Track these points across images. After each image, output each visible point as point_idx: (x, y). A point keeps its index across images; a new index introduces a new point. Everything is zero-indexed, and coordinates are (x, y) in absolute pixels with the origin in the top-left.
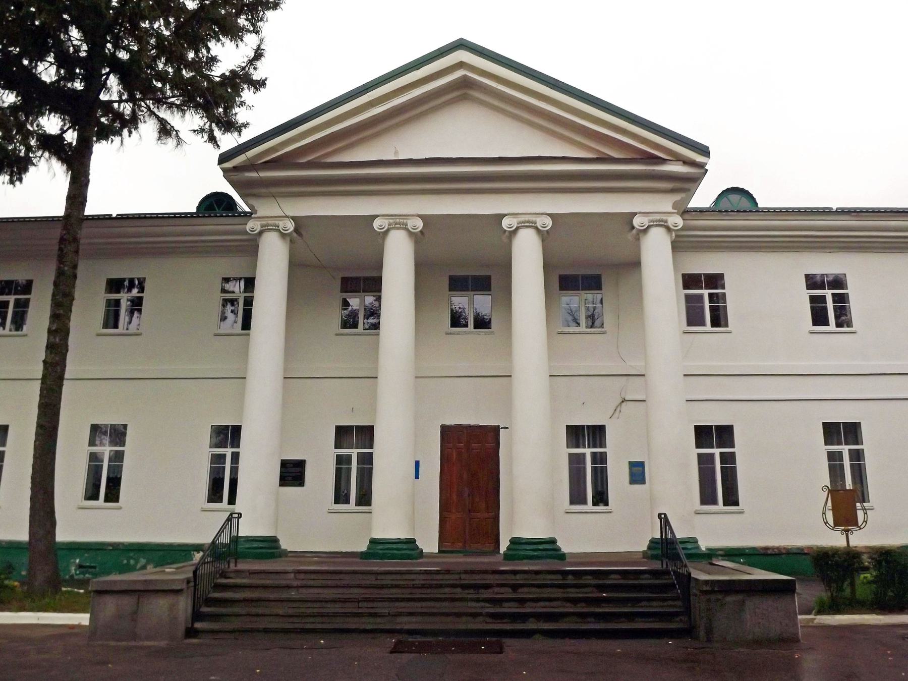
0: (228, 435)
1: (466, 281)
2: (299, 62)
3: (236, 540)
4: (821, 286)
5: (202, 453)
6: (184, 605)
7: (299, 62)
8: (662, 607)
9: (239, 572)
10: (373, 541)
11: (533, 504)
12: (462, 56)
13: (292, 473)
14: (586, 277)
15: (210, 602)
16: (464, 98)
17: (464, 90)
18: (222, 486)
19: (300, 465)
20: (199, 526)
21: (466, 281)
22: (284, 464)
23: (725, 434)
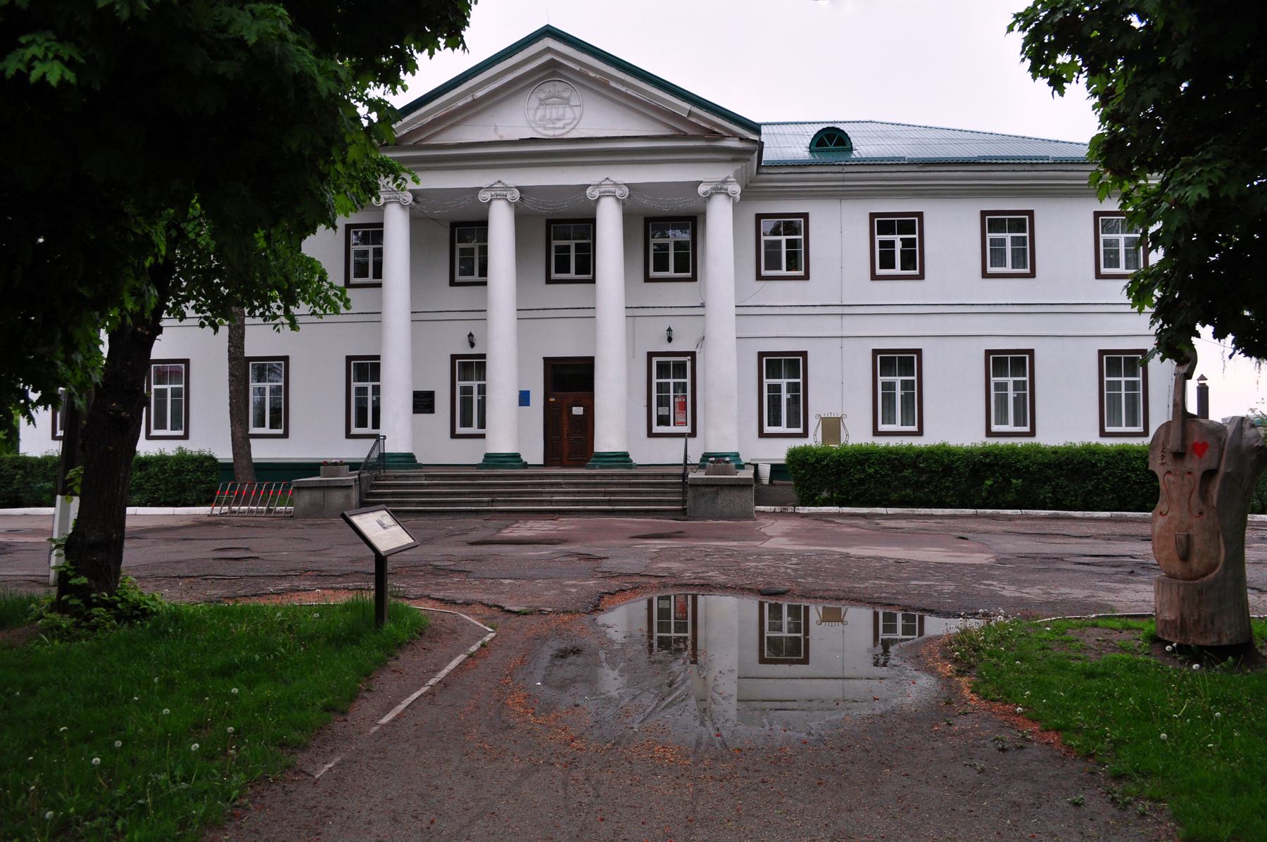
0: (365, 369)
1: (562, 243)
2: (491, 27)
3: (383, 456)
7: (491, 27)
9: (387, 478)
10: (488, 456)
11: (617, 423)
13: (423, 402)
15: (369, 495)
16: (554, 74)
17: (552, 70)
19: (431, 395)
20: (358, 451)
21: (562, 243)
22: (416, 395)
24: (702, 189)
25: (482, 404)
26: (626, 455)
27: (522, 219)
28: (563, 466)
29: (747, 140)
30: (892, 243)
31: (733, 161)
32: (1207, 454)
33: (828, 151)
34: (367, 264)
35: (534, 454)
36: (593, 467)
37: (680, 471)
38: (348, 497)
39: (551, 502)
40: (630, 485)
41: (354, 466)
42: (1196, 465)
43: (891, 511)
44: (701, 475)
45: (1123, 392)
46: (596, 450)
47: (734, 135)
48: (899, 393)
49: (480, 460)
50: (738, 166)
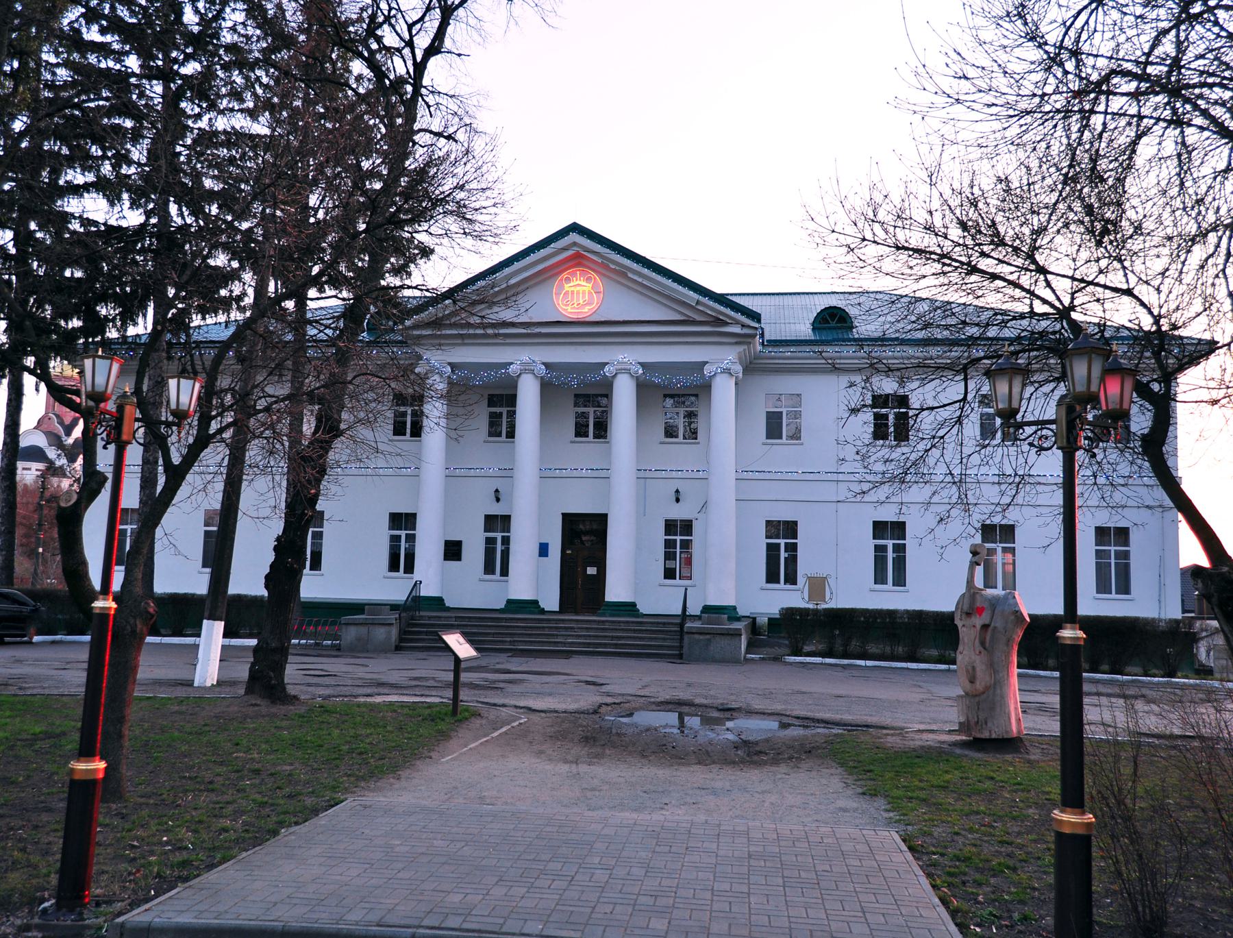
0: (403, 521)
4: (885, 405)
5: (383, 533)
6: (394, 632)
8: (867, 701)
9: (421, 617)
10: (509, 602)
11: (628, 575)
12: (574, 237)
13: (453, 551)
14: (677, 401)
16: (579, 264)
17: (578, 260)
18: (401, 559)
20: (395, 590)
23: (790, 529)
24: (707, 370)
25: (506, 555)
26: (633, 605)
27: (547, 388)
28: (577, 613)
29: (749, 327)
30: (886, 417)
31: (736, 343)
32: (984, 614)
33: (830, 328)
34: (405, 423)
35: (551, 601)
36: (603, 615)
37: (678, 621)
38: (389, 632)
39: (564, 644)
40: (635, 631)
41: (394, 607)
42: (978, 621)
43: (870, 663)
44: (697, 624)
45: (1113, 561)
46: (607, 599)
47: (737, 322)
48: (890, 555)
49: (502, 605)
50: (741, 348)
